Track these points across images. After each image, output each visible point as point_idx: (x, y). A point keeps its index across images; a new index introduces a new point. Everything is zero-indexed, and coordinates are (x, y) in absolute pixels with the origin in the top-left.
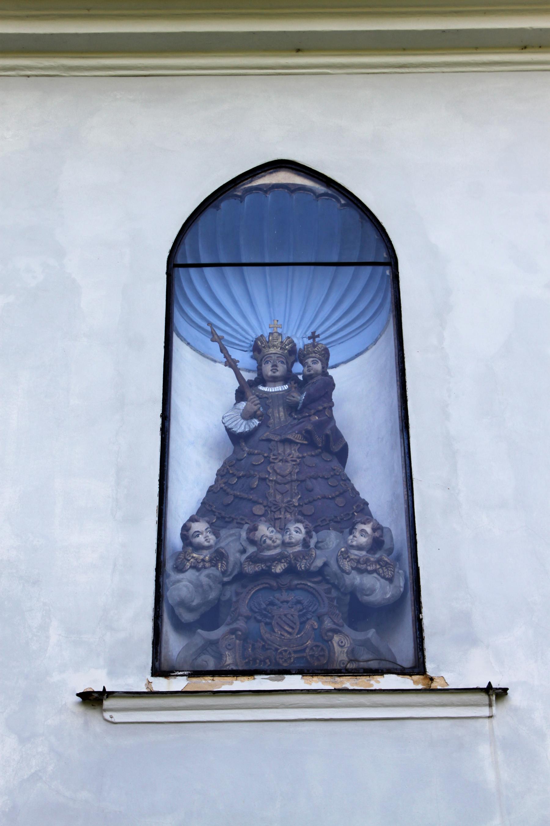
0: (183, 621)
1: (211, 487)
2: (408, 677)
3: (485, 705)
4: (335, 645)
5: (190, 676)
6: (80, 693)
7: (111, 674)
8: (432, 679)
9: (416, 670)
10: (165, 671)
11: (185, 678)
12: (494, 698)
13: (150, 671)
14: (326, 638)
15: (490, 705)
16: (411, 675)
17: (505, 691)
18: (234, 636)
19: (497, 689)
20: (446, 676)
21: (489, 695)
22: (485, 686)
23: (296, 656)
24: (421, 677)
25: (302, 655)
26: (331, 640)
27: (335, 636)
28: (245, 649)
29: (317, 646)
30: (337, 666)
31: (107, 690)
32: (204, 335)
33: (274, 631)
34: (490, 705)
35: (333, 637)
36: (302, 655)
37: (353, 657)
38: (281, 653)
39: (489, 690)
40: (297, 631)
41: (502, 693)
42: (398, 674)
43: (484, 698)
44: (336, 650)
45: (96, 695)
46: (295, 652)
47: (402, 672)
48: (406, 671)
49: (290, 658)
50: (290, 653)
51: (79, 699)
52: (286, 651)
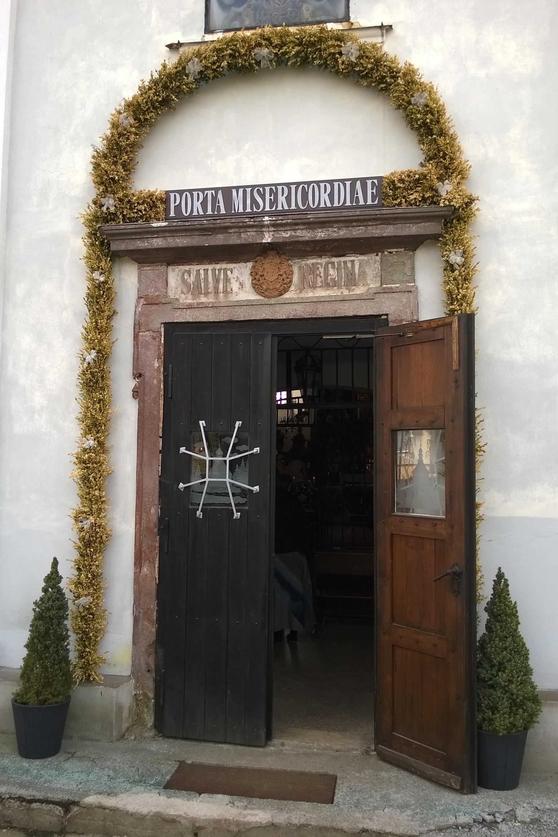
0: (225, 3)
1: (526, 657)
2: (340, 23)
3: (379, 36)
4: (304, 10)
5: (224, 32)
6: (169, 45)
7: (184, 34)
8: (352, 24)
9: (344, 20)
10: (211, 31)
11: (222, 33)
12: (385, 31)
13: (204, 31)
14: (298, 6)
15: (383, 36)
16: (341, 22)
17: (391, 26)
18: (250, 9)
19: (386, 26)
20: (358, 20)
21: (382, 30)
22: (380, 25)
23: (282, 17)
24: (347, 23)
25: (285, 17)
26: (301, 7)
27: (304, 4)
28: (255, 16)
29: (294, 11)
30: (304, 21)
31: (181, 42)
32: (377, 604)
33: (270, 4)
34: (383, 36)
35: (302, 6)
36: (285, 17)
37: (313, 14)
38: (274, 16)
39: (381, 27)
40: (282, 3)
41: (390, 28)
42: (334, 22)
43: (379, 32)
44: (304, 12)
45: (175, 46)
46: (282, 15)
47: (337, 21)
48: (339, 20)
49: (279, 19)
50: (279, 16)
51: (168, 49)
52: (276, 15)
